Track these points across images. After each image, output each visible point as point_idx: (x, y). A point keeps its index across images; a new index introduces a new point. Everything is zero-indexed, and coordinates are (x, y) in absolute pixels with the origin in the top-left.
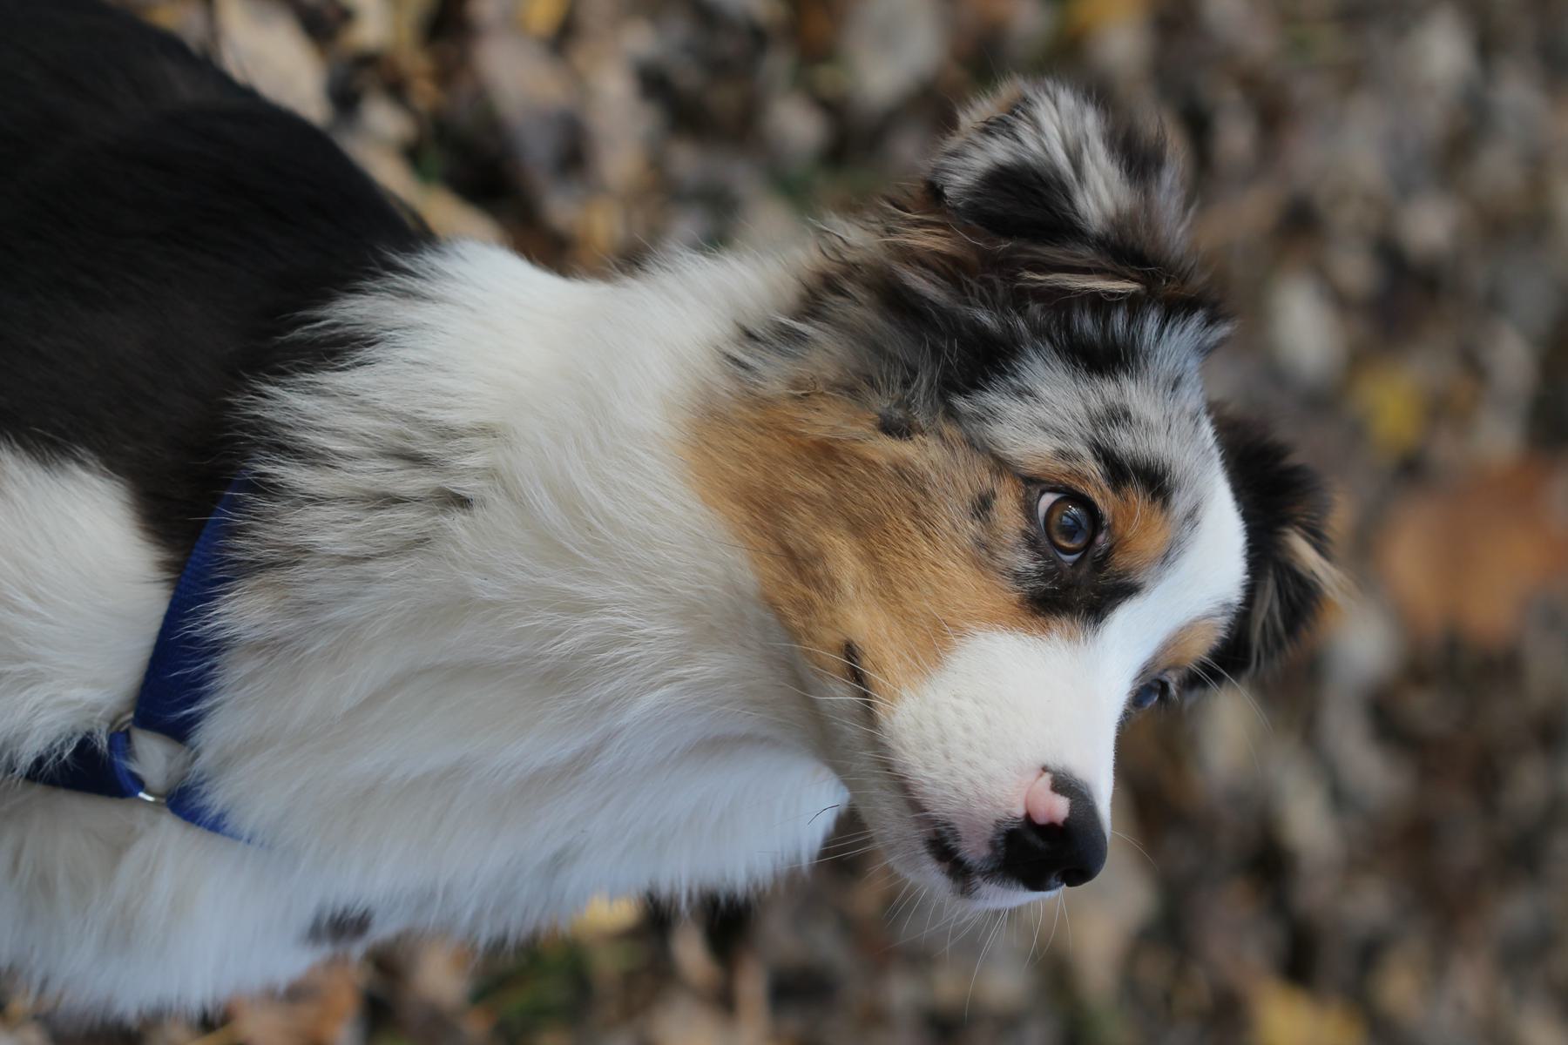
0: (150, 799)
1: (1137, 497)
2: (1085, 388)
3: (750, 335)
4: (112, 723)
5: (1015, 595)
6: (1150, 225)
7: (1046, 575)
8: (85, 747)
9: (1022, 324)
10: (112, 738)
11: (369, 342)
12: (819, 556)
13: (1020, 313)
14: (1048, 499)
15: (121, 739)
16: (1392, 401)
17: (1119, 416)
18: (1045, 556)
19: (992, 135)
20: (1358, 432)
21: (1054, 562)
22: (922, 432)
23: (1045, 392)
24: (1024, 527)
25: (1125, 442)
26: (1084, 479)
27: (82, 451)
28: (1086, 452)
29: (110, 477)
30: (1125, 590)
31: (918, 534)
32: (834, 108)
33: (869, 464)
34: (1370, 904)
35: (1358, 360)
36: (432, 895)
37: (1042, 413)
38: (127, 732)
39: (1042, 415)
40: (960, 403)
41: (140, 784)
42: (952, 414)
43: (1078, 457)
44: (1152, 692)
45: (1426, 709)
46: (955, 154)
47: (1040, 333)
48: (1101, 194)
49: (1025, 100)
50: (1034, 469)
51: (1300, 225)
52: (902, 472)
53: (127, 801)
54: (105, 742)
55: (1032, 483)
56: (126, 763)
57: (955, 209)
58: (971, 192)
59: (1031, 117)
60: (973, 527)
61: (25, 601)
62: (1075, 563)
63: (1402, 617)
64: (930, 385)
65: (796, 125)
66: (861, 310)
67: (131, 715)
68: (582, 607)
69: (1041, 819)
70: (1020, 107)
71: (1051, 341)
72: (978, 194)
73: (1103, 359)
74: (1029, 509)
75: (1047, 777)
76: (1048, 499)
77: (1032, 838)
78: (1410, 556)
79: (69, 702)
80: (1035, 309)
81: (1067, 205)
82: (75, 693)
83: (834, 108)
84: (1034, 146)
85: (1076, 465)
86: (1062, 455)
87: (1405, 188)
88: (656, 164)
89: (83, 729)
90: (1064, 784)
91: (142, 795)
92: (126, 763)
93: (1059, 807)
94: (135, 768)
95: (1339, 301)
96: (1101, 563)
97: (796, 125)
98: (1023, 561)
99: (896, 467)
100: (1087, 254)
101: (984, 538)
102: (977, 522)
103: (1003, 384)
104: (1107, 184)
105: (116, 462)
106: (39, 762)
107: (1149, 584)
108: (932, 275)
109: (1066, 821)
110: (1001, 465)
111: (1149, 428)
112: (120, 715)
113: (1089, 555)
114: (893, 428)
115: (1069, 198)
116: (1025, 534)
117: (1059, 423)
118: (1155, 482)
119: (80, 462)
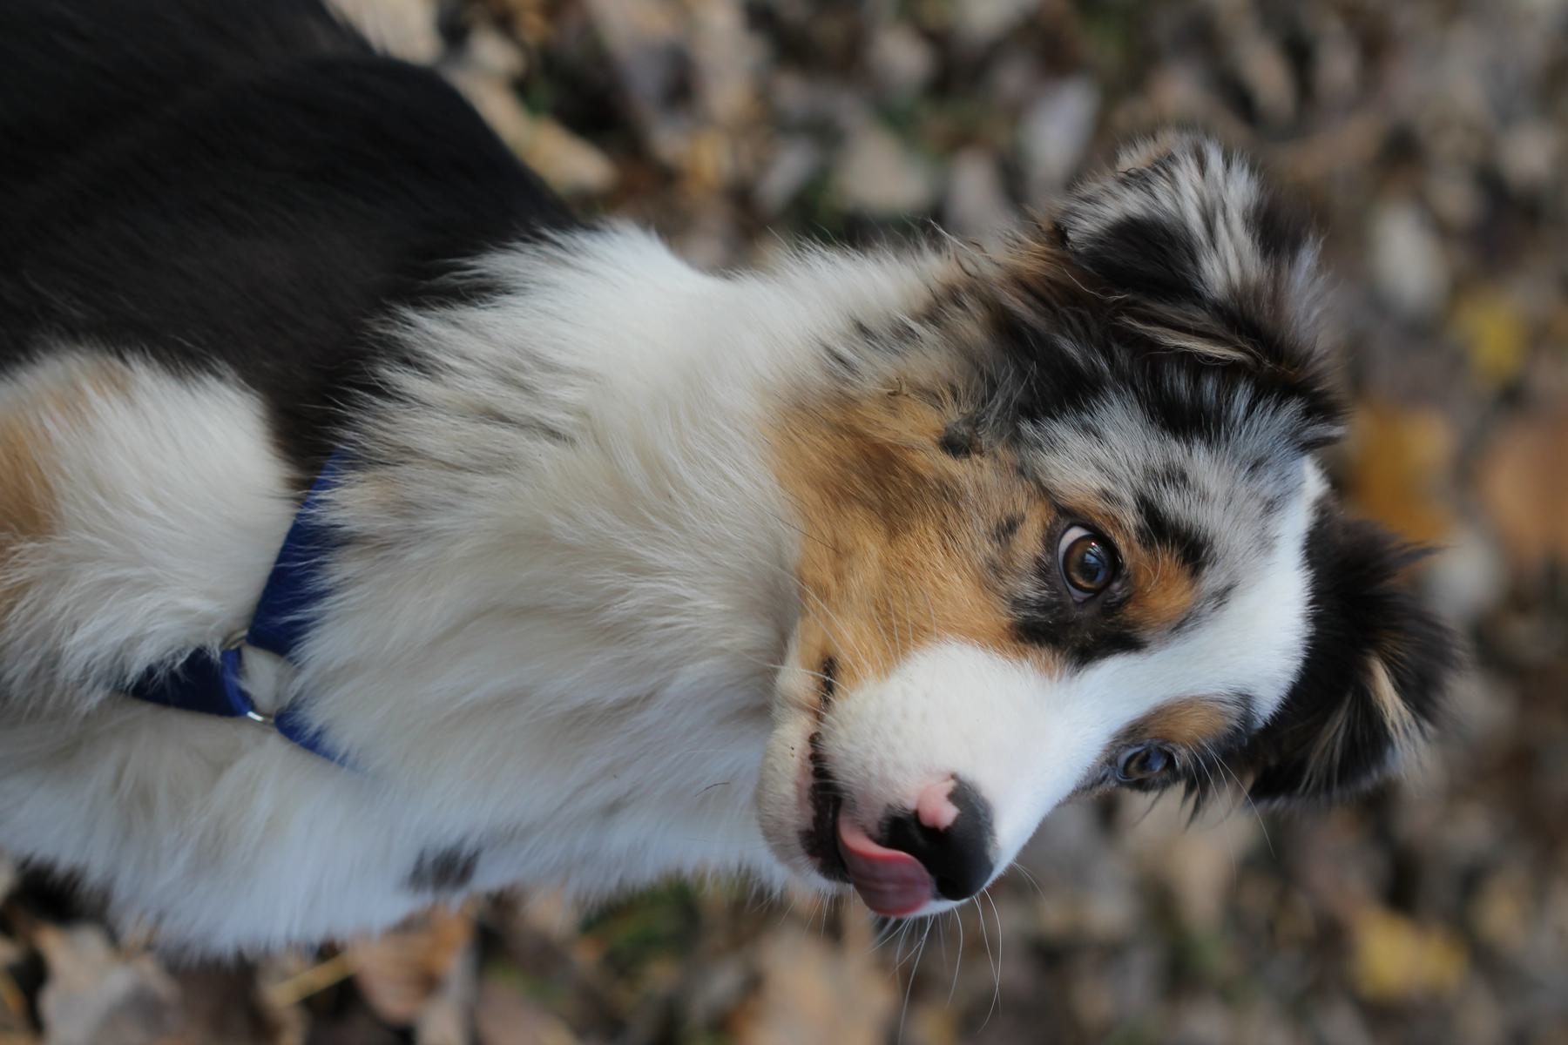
0: (259, 718)
1: (1167, 559)
2: (1155, 445)
3: (863, 330)
4: (225, 641)
5: (1008, 620)
6: (1276, 300)
7: (1044, 607)
8: (198, 661)
9: (1104, 365)
10: (224, 654)
11: (507, 291)
12: (849, 553)
13: (1104, 354)
14: (1075, 533)
15: (234, 658)
16: (1494, 329)
17: (1177, 477)
18: (1051, 585)
19: (1127, 186)
20: (1458, 361)
21: (1059, 595)
22: (981, 453)
23: (1111, 435)
24: (1039, 554)
25: (1173, 503)
26: (1116, 523)
27: (223, 366)
28: (1128, 498)
29: (246, 390)
30: (1124, 640)
31: (937, 544)
32: (938, 39)
33: (918, 478)
34: (1471, 831)
35: (1459, 288)
36: (1340, 781)
37: (1101, 454)
38: (238, 652)
39: (1101, 458)
40: (1027, 428)
41: (248, 702)
42: (1016, 439)
43: (1119, 501)
44: (1143, 757)
45: (1527, 636)
46: (1088, 200)
47: (1124, 379)
48: (1229, 262)
49: (1171, 158)
50: (1069, 503)
51: (1401, 154)
52: (948, 493)
53: (235, 720)
54: (218, 654)
55: (1068, 514)
56: (236, 680)
57: (1076, 253)
58: (1094, 239)
59: (1171, 174)
60: (988, 549)
61: (148, 505)
62: (1086, 601)
63: (1503, 543)
64: (1005, 406)
65: (901, 56)
66: (971, 327)
67: (245, 633)
68: (638, 569)
69: (926, 822)
70: (1164, 165)
71: (1135, 389)
72: (1101, 242)
73: (1182, 419)
74: (1051, 540)
75: (952, 784)
76: (1075, 533)
77: (916, 833)
78: (1511, 485)
79: (189, 612)
80: (1122, 356)
81: (1190, 265)
82: (191, 602)
83: (938, 39)
84: (1167, 203)
85: (1115, 510)
86: (1106, 495)
87: (1506, 117)
88: (763, 95)
89: (196, 642)
90: (963, 794)
91: (251, 715)
92: (236, 680)
93: (947, 814)
94: (245, 686)
95: (1440, 229)
96: (1111, 609)
97: (901, 56)
98: (1028, 588)
99: (940, 483)
100: (1202, 318)
101: (999, 560)
102: (996, 545)
103: (1072, 419)
104: (1239, 255)
105: (253, 378)
106: (150, 671)
107: (1152, 646)
108: (1030, 299)
109: (948, 829)
110: (1045, 493)
111: (1204, 497)
112: (233, 633)
113: (1100, 598)
114: (954, 445)
115: (1194, 260)
116: (1038, 561)
117: (1114, 465)
118: (1193, 551)
119: (220, 377)
